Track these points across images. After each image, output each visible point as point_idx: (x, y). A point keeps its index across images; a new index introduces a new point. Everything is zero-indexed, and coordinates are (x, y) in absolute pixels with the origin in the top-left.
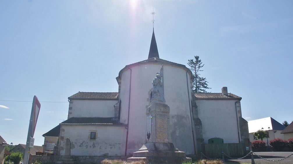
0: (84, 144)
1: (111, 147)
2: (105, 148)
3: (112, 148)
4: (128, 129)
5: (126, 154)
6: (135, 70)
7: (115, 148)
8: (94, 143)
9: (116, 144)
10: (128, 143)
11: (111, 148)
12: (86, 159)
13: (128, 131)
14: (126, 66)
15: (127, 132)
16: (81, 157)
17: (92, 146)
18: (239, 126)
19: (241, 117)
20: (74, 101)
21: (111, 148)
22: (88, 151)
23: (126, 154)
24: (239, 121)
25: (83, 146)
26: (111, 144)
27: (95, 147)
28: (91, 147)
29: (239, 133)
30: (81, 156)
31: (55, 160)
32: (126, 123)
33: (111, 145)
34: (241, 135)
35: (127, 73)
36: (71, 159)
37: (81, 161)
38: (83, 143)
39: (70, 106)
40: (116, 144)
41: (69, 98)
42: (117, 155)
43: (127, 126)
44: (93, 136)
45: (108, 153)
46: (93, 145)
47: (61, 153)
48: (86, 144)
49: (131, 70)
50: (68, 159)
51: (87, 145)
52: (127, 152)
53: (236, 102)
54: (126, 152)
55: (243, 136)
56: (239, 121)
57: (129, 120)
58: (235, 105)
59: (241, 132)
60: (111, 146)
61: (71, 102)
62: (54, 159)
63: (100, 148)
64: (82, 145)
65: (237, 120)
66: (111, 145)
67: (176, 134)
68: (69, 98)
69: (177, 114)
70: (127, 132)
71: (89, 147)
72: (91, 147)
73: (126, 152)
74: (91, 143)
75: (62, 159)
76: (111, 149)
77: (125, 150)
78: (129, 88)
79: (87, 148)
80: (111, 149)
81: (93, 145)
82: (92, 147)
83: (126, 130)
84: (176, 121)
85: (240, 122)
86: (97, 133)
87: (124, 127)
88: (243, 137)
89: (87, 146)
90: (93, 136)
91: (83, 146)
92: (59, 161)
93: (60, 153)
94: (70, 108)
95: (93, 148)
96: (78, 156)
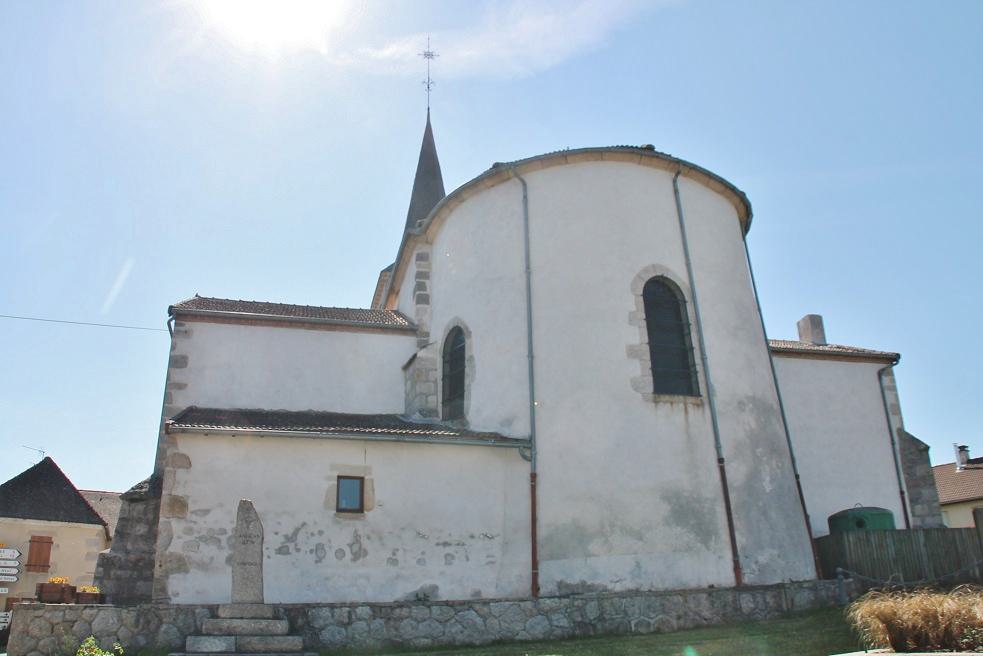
0: (301, 537)
1: (447, 555)
2: (419, 561)
3: (453, 557)
4: (531, 459)
5: (535, 587)
6: (536, 179)
7: (468, 559)
8: (356, 531)
9: (472, 537)
10: (542, 533)
11: (449, 559)
12: (350, 623)
13: (534, 467)
14: (496, 166)
15: (534, 477)
16: (326, 612)
17: (347, 550)
18: (900, 464)
19: (901, 431)
20: (197, 327)
21: (449, 559)
22: (327, 579)
23: (535, 587)
24: (897, 447)
25: (298, 550)
26: (448, 540)
27: (366, 553)
28: (340, 554)
29: (902, 493)
30: (325, 606)
31: (164, 628)
32: (520, 430)
33: (446, 544)
34: (911, 501)
35: (732, 218)
36: (282, 626)
37: (326, 635)
38: (297, 530)
39: (177, 353)
40: (472, 537)
41: (171, 310)
42: (478, 593)
43: (530, 448)
44: (351, 497)
45: (435, 588)
46: (350, 546)
47: (170, 591)
48: (316, 540)
49: (524, 184)
50: (264, 623)
51: (319, 548)
52: (540, 580)
53: (883, 370)
54: (535, 576)
55: (919, 506)
56: (897, 447)
57: (537, 417)
58: (877, 384)
59: (908, 487)
60: (448, 550)
61: (182, 328)
62: (158, 627)
63: (393, 561)
64: (291, 546)
65: (893, 444)
66: (446, 544)
67: (764, 484)
68: (171, 310)
69: (751, 394)
70: (534, 477)
71: (331, 555)
72: (340, 554)
73: (535, 576)
74: (340, 534)
75: (225, 624)
76: (448, 563)
77: (526, 571)
78: (520, 266)
79: (319, 561)
80: (448, 563)
81: (350, 546)
82: (349, 556)
83: (526, 468)
84: (753, 425)
85: (902, 450)
86: (372, 481)
87: (515, 452)
88: (918, 508)
89: (319, 551)
90: (351, 497)
91: (298, 550)
92: (211, 639)
93: (164, 590)
94: (177, 362)
95: (356, 557)
96: (308, 605)
